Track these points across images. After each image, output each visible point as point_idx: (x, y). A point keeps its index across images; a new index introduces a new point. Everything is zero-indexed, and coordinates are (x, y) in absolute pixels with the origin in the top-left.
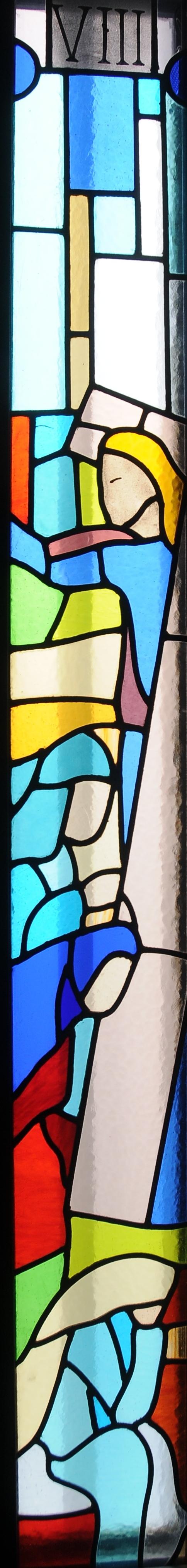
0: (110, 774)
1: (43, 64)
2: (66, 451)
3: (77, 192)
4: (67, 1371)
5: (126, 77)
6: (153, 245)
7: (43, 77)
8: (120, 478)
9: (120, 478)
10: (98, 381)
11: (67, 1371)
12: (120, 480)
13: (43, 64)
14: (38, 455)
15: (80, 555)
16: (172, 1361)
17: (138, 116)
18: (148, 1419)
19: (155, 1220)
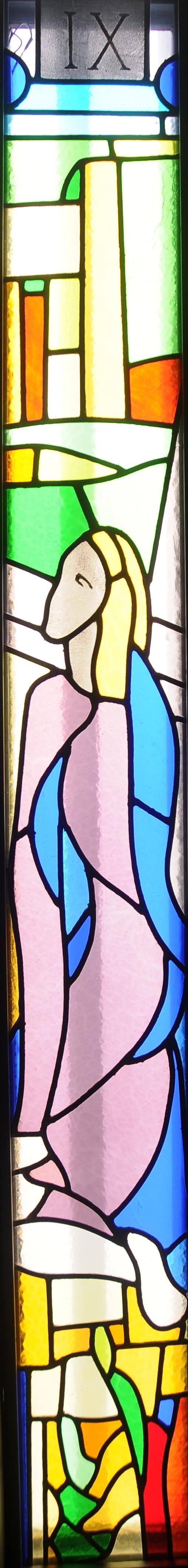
0: (125, 697)
1: (33, 73)
2: (42, 1133)
3: (92, 1498)
4: (155, 626)
5: (57, 573)
6: (36, 1428)
7: (34, 87)
8: (91, 587)
9: (91, 587)
10: (39, 1139)
11: (155, 626)
12: (80, 586)
13: (33, 73)
15: (36, 791)
16: (175, 1398)
17: (126, 702)
18: (30, 81)
19: (29, 418)
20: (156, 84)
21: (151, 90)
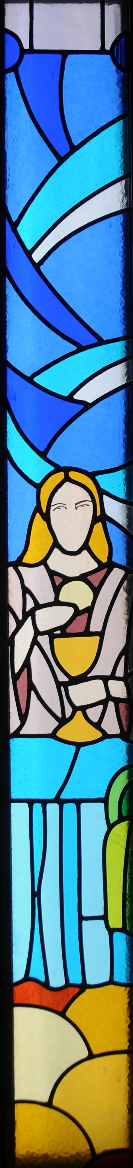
1: (26, 46)
14: (29, 247)
20: (110, 52)
21: (108, 57)
